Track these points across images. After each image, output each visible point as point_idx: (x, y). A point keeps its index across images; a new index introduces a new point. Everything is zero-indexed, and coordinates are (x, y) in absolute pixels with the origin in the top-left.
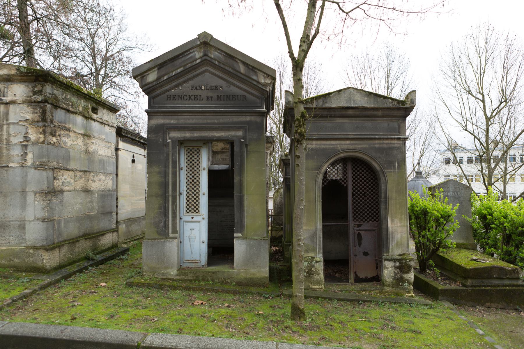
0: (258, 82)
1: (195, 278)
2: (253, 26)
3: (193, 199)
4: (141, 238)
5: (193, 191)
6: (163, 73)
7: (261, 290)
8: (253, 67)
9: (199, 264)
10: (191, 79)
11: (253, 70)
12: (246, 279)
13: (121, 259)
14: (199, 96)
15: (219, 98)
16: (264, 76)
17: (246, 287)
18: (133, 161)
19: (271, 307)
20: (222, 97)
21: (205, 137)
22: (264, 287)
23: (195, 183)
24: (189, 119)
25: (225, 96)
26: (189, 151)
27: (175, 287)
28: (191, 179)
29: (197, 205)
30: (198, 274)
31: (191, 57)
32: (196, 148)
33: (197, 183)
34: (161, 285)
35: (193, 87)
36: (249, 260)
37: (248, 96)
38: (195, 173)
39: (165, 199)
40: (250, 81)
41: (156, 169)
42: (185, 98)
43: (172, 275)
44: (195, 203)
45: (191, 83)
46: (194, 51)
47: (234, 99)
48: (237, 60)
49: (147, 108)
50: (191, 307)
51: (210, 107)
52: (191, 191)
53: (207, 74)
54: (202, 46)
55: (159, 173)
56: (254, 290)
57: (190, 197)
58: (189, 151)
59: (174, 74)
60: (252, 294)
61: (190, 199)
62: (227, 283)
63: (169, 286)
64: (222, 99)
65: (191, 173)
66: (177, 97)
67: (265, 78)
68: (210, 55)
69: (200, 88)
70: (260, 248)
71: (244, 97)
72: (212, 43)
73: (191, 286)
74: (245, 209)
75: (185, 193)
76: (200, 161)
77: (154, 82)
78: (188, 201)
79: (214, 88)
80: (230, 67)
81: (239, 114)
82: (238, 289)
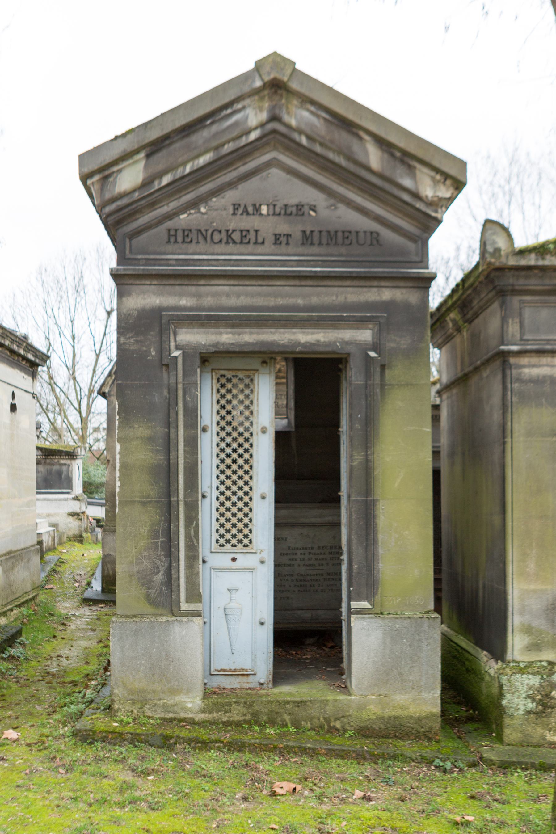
0: (416, 196)
1: (248, 717)
2: (447, 28)
3: (234, 510)
4: (31, 600)
5: (234, 488)
6: (161, 167)
7: (428, 749)
8: (405, 153)
9: (251, 678)
10: (231, 185)
11: (402, 162)
12: (381, 719)
13: (12, 658)
14: (252, 233)
15: (307, 238)
16: (433, 178)
17: (381, 742)
18: (13, 408)
19: (472, 797)
20: (316, 235)
21: (272, 343)
22: (430, 739)
23: (241, 467)
24: (228, 295)
25: (324, 234)
26: (223, 381)
27: (204, 743)
28: (229, 456)
29: (246, 526)
30: (257, 708)
31: (236, 124)
32: (241, 375)
33: (246, 467)
34: (167, 738)
35: (236, 207)
36: (389, 672)
37: (386, 234)
38: (241, 440)
39: (168, 510)
40: (396, 191)
41: (141, 430)
42: (217, 237)
43: (190, 710)
44: (240, 520)
45: (231, 196)
46: (244, 108)
47: (347, 242)
48: (362, 134)
49: (114, 265)
50: (271, 800)
51: (284, 263)
52: (228, 488)
53: (274, 171)
54: (266, 92)
55: (150, 440)
56: (410, 748)
57: (228, 504)
58: (223, 381)
59: (188, 169)
60: (406, 759)
61: (228, 510)
62: (332, 730)
63: (189, 741)
64: (316, 239)
65: (229, 440)
66: (194, 235)
67: (436, 183)
68: (286, 118)
69: (257, 209)
70: (420, 641)
71: (375, 237)
72: (294, 85)
73: (246, 738)
74: (380, 537)
75: (216, 493)
76: (254, 408)
77: (134, 191)
78: (222, 515)
79: (294, 210)
80: (340, 152)
81: (362, 283)
82: (367, 746)
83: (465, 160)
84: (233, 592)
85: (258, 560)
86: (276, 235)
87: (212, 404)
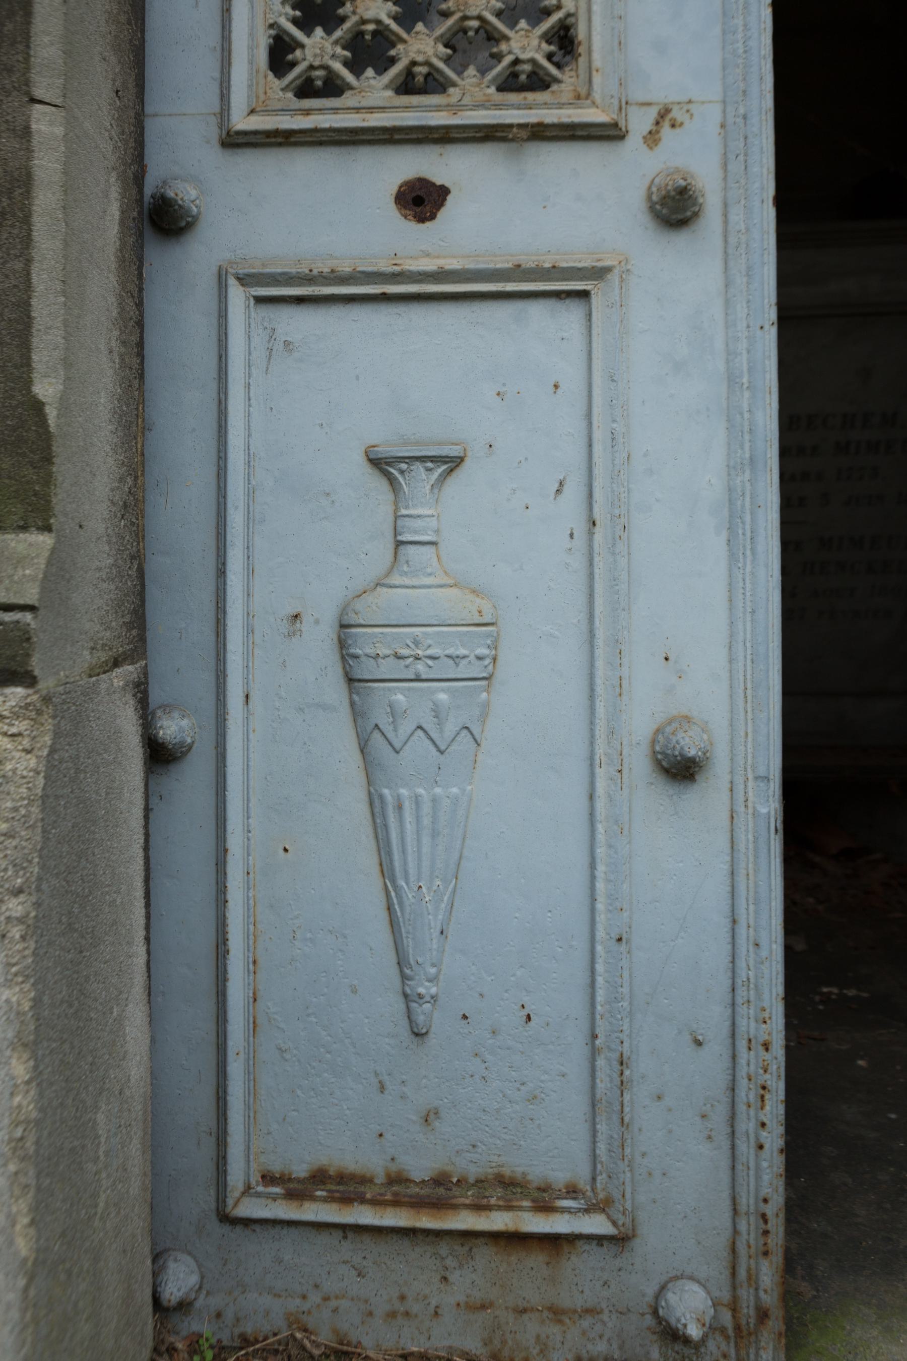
83: (442, 214)
84: (421, 480)
85: (636, 199)
86: (439, 1118)
87: (540, 133)
